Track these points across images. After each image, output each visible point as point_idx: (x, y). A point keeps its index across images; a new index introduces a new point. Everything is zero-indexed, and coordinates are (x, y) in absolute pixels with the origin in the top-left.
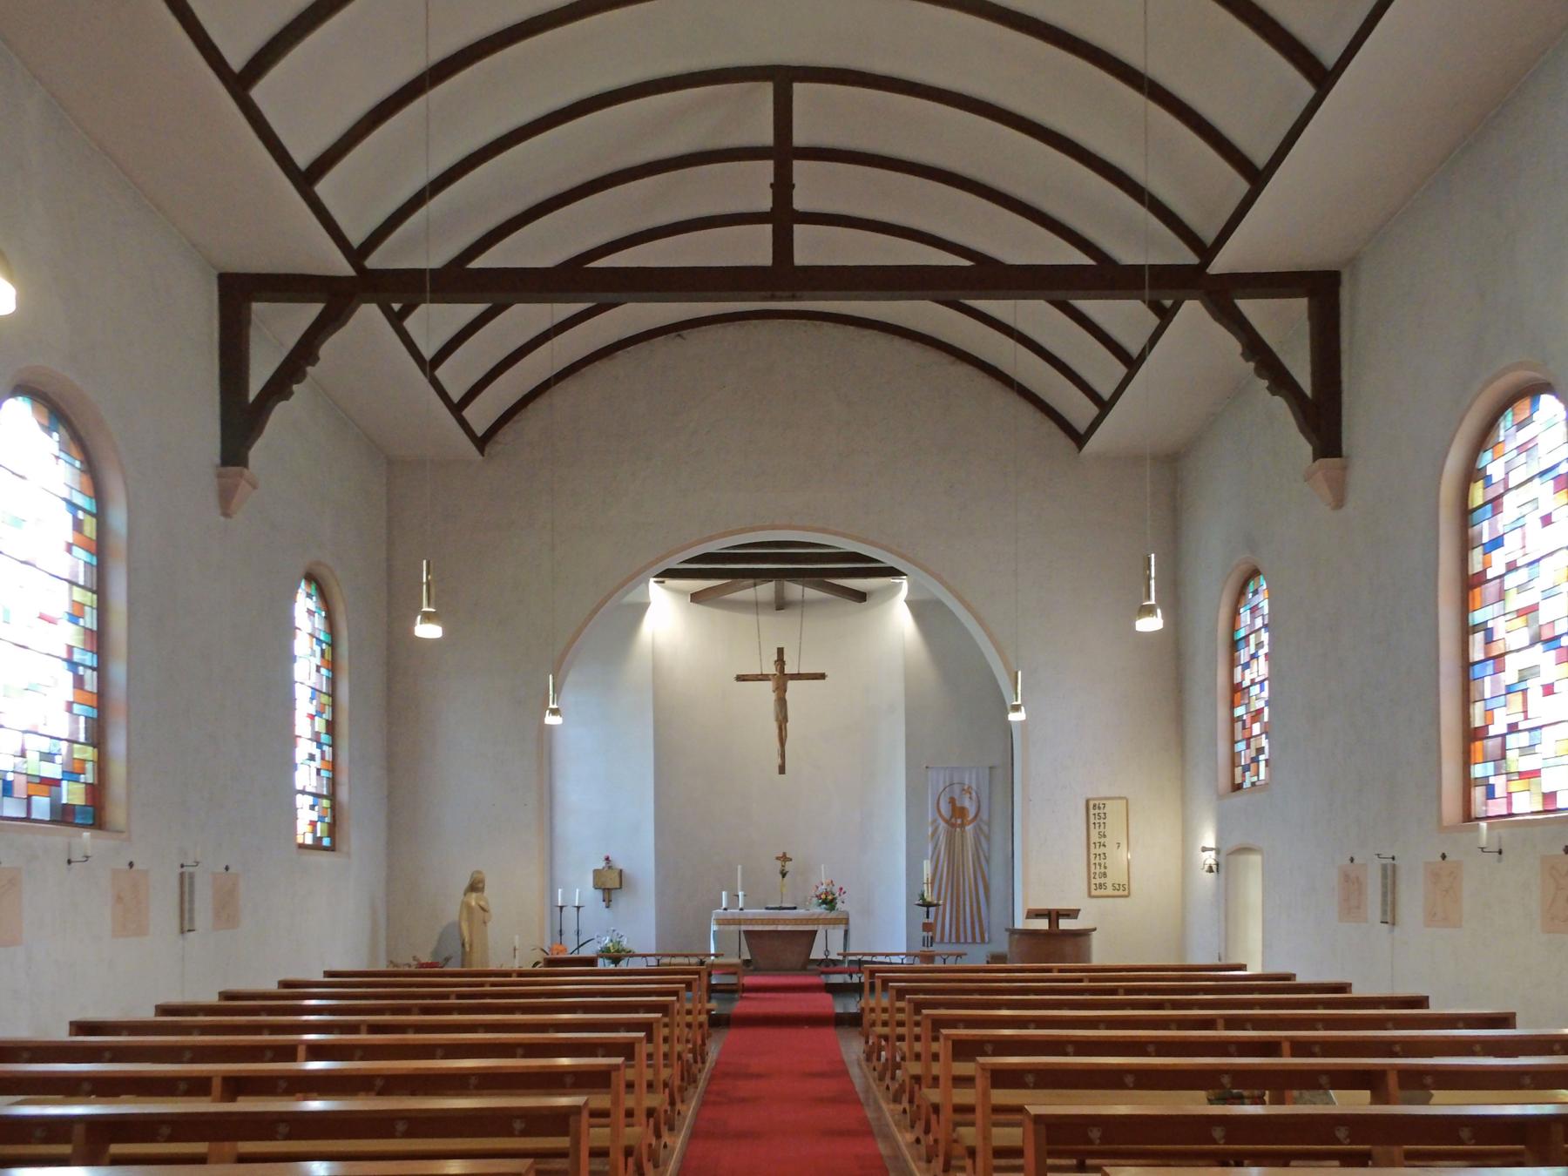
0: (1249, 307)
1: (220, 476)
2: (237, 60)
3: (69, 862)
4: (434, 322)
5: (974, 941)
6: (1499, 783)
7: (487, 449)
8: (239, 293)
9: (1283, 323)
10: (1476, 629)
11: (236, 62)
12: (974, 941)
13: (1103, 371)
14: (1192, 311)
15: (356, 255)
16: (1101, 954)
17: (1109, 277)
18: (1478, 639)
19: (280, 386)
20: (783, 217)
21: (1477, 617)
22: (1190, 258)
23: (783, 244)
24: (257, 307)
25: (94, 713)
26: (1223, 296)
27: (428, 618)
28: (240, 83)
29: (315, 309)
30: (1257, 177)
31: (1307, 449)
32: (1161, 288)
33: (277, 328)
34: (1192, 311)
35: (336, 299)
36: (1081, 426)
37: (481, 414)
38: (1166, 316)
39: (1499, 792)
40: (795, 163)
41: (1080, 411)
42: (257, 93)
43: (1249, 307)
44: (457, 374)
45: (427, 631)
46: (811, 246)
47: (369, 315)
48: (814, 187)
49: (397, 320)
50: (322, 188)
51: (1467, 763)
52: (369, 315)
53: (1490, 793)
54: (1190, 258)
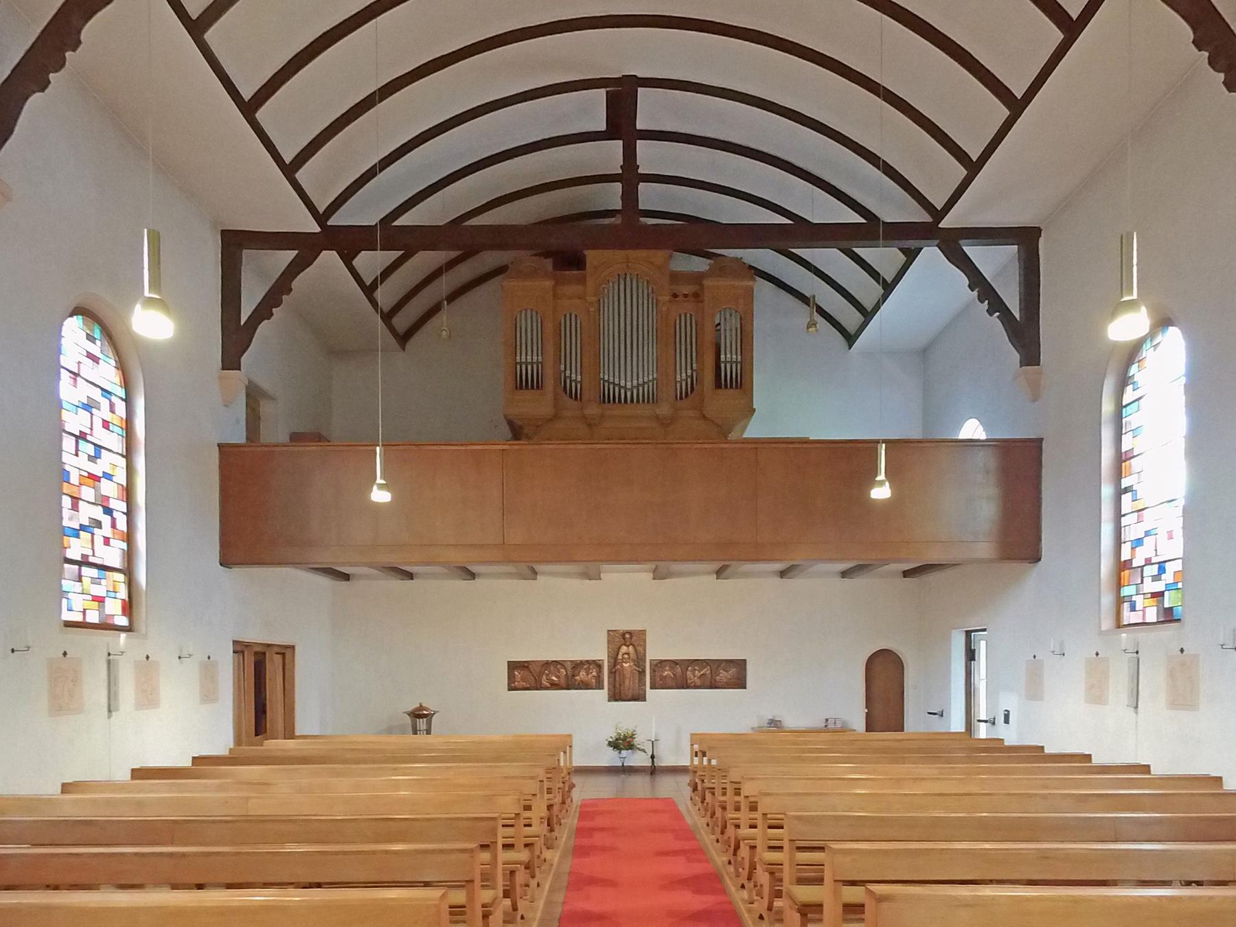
0: (973, 251)
1: (220, 378)
2: (247, 93)
3: (13, 651)
4: (370, 262)
5: (532, 387)
6: (1139, 600)
7: (408, 347)
8: (235, 243)
9: (994, 261)
10: (1126, 490)
11: (247, 94)
12: (532, 387)
13: (866, 290)
14: (931, 254)
15: (321, 218)
16: (1046, 751)
17: (871, 229)
18: (1126, 498)
19: (263, 311)
20: (630, 176)
21: (1125, 483)
22: (926, 218)
23: (630, 196)
24: (246, 253)
25: (124, 546)
26: (953, 246)
27: (381, 487)
28: (249, 108)
29: (291, 254)
30: (973, 167)
31: (1016, 356)
32: (909, 238)
33: (261, 272)
34: (931, 254)
35: (306, 249)
36: (852, 329)
37: (402, 321)
38: (911, 255)
39: (1139, 606)
40: (638, 142)
41: (850, 318)
42: (260, 115)
43: (973, 251)
44: (386, 295)
45: (380, 496)
46: (649, 196)
47: (329, 259)
48: (649, 156)
49: (348, 259)
50: (300, 175)
51: (1119, 586)
52: (329, 259)
53: (1133, 609)
54: (926, 218)
